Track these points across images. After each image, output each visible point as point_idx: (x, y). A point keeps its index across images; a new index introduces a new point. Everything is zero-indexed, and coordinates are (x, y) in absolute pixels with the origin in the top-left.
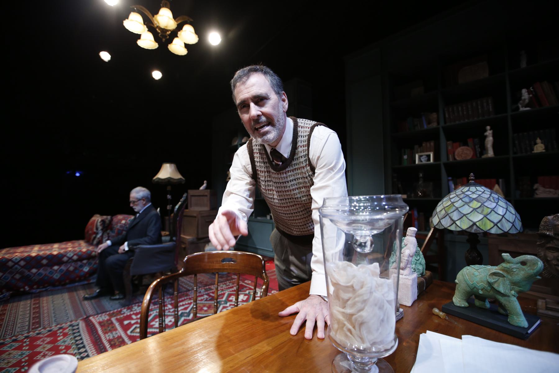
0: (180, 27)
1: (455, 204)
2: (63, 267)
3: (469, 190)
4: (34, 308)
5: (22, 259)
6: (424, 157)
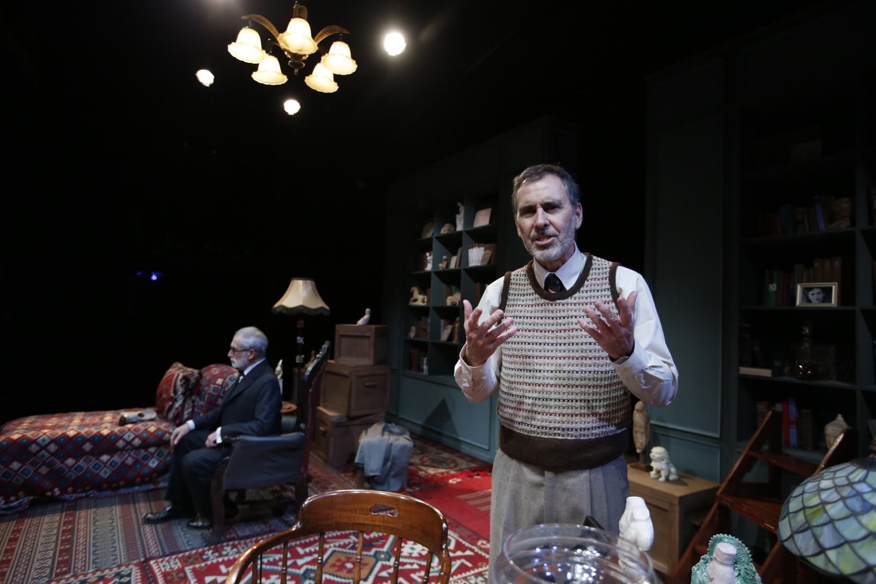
0: (324, 47)
1: (828, 507)
2: (116, 458)
3: (863, 480)
4: (64, 532)
5: (53, 441)
6: (816, 291)
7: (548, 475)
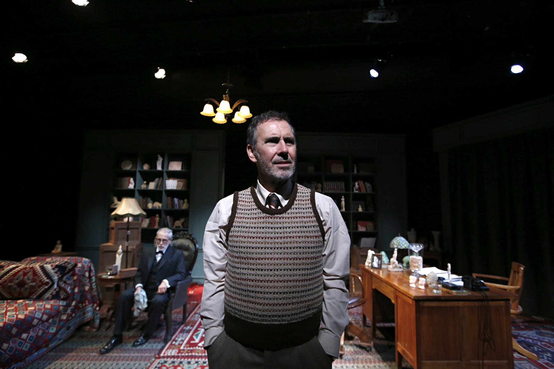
7: (267, 353)
